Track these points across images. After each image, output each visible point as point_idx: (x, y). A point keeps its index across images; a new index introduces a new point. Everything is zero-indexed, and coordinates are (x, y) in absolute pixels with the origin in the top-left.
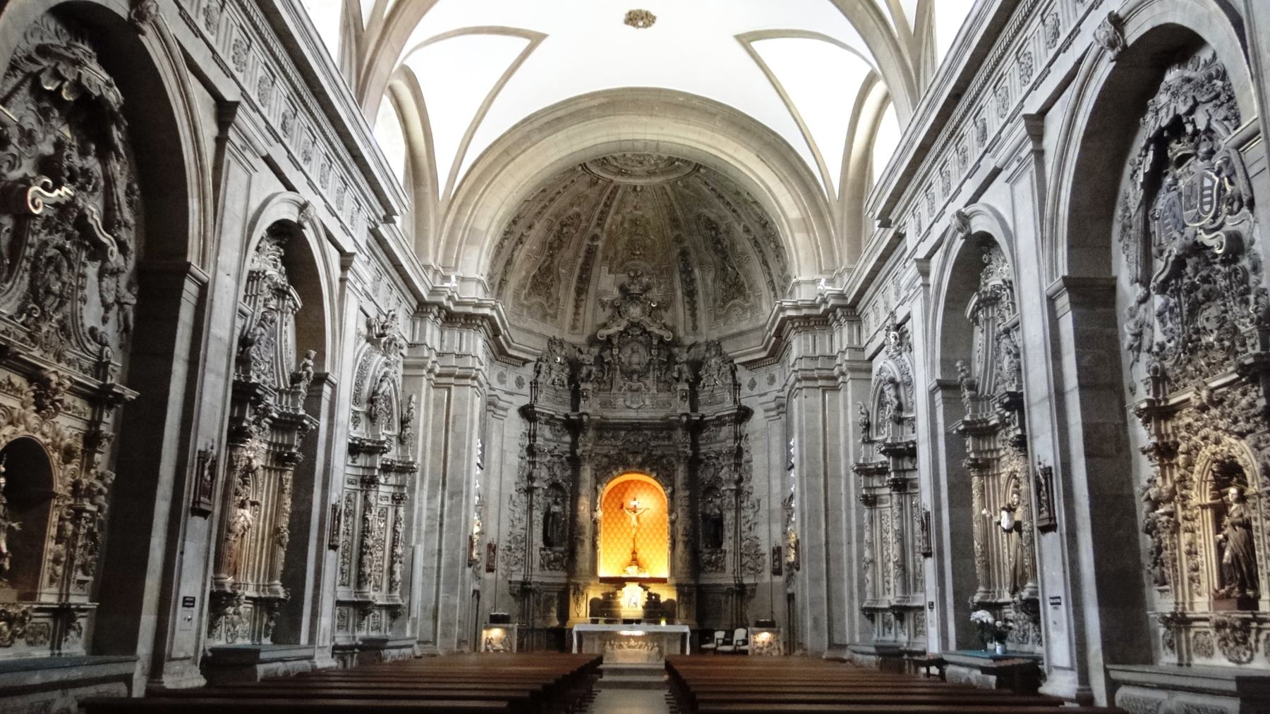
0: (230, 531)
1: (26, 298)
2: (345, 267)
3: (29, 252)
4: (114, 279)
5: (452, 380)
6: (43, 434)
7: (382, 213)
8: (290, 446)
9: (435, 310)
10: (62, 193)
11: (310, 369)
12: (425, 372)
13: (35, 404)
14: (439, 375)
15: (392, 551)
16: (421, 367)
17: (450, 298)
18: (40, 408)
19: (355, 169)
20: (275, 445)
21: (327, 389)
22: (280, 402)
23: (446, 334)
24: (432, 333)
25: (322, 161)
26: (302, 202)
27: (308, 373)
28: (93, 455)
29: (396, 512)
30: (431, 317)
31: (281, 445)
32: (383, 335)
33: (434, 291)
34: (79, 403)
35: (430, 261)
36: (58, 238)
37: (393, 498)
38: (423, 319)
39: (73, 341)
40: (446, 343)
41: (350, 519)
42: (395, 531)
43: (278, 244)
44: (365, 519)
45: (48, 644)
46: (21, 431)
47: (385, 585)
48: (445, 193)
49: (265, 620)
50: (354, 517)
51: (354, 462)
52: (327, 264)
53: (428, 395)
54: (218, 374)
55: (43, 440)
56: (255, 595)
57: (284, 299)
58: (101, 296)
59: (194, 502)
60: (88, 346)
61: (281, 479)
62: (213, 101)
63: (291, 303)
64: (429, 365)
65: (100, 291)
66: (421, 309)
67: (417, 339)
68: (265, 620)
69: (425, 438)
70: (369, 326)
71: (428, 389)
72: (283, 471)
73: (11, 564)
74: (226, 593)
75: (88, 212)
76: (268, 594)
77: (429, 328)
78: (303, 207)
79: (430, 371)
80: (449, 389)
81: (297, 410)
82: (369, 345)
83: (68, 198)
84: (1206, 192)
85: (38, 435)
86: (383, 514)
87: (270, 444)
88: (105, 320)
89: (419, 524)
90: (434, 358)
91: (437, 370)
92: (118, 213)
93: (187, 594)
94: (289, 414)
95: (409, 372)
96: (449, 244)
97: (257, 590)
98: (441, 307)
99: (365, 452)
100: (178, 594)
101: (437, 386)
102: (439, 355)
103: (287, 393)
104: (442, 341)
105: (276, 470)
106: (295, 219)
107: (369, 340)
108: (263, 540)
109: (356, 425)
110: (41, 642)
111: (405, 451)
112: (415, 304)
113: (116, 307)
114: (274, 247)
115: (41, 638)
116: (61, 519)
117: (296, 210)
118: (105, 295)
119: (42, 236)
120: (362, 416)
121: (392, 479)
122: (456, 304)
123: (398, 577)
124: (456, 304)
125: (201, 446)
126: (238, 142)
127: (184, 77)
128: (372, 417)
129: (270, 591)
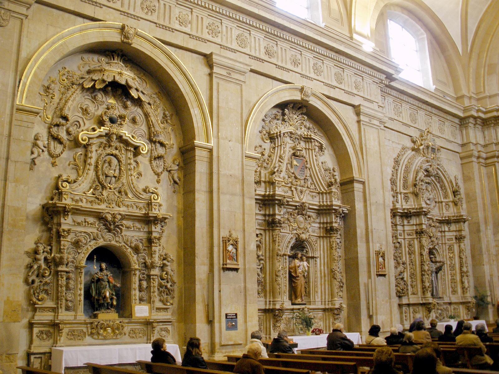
0: (277, 276)
1: (94, 182)
2: (358, 114)
3: (93, 161)
4: (162, 160)
5: (496, 159)
6: (117, 242)
7: (383, 77)
8: (331, 223)
9: (471, 120)
10: (102, 130)
11: (337, 177)
12: (474, 159)
13: (106, 229)
14: (486, 159)
15: (461, 270)
16: (471, 156)
17: (478, 111)
18: (110, 231)
19: (342, 58)
20: (323, 223)
21: (357, 186)
22: (323, 199)
23: (486, 132)
24: (475, 135)
25: (312, 62)
26: (300, 88)
27: (336, 180)
28: (151, 248)
29: (459, 246)
30: (472, 126)
31: (327, 223)
32: (422, 145)
33: (465, 110)
34: (138, 225)
35: (464, 92)
36: (108, 151)
37: (456, 238)
38: (466, 127)
39: (130, 195)
40: (487, 138)
41: (413, 256)
42: (460, 257)
43: (302, 114)
44: (421, 255)
45: (145, 338)
46: (101, 243)
47: (459, 290)
48: (462, 50)
49: (331, 320)
50: (414, 254)
51: (409, 222)
52: (342, 118)
53: (480, 172)
54: (233, 194)
55: (118, 244)
56: (323, 307)
57: (311, 142)
58: (153, 170)
59: (223, 265)
60: (141, 196)
61: (330, 242)
62: (202, 57)
63: (317, 144)
64: (476, 154)
65: (152, 168)
66: (463, 122)
67: (465, 141)
68: (331, 320)
69: (483, 198)
70: (414, 142)
71: (479, 169)
72: (330, 237)
73: (492, 357)
74: (279, 310)
75: (122, 134)
76: (330, 306)
77: (471, 132)
78: (302, 90)
79: (479, 157)
80: (495, 165)
81: (331, 201)
82: (414, 153)
83: (107, 131)
84: (228, 14)
85: (113, 243)
86: (451, 249)
87: (320, 223)
88: (158, 182)
89: (488, 251)
90: (480, 148)
91: (484, 155)
92: (153, 129)
93: (228, 311)
94: (324, 206)
95: (465, 161)
96: (477, 78)
97: (325, 304)
98: (475, 118)
99: (414, 215)
100: (220, 312)
101: (487, 165)
102: (485, 146)
103: (326, 193)
104: (485, 137)
105: (326, 237)
106: (299, 98)
107: (413, 149)
108: (325, 276)
109: (407, 202)
110: (141, 337)
111: (458, 209)
112: (457, 121)
113: (166, 174)
114: (300, 116)
115: (141, 335)
116: (140, 280)
117: (299, 93)
118: (155, 169)
119: (98, 152)
120: (409, 195)
121: (453, 227)
122: (485, 113)
123: (427, 284)
124: (485, 113)
125: (224, 233)
126: (224, 72)
127: (164, 49)
128: (416, 195)
129: (332, 304)
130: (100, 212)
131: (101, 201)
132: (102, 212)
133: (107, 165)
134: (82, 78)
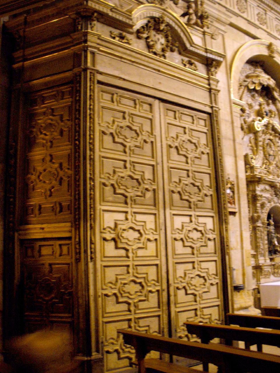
46: (273, 204)
130: (273, 182)
131: (270, 173)
132: (274, 182)
133: (268, 147)
134: (245, 81)
